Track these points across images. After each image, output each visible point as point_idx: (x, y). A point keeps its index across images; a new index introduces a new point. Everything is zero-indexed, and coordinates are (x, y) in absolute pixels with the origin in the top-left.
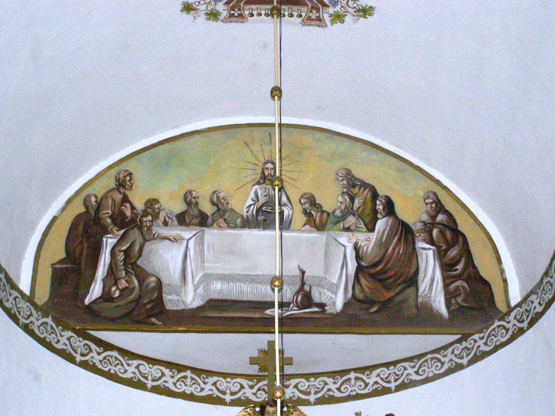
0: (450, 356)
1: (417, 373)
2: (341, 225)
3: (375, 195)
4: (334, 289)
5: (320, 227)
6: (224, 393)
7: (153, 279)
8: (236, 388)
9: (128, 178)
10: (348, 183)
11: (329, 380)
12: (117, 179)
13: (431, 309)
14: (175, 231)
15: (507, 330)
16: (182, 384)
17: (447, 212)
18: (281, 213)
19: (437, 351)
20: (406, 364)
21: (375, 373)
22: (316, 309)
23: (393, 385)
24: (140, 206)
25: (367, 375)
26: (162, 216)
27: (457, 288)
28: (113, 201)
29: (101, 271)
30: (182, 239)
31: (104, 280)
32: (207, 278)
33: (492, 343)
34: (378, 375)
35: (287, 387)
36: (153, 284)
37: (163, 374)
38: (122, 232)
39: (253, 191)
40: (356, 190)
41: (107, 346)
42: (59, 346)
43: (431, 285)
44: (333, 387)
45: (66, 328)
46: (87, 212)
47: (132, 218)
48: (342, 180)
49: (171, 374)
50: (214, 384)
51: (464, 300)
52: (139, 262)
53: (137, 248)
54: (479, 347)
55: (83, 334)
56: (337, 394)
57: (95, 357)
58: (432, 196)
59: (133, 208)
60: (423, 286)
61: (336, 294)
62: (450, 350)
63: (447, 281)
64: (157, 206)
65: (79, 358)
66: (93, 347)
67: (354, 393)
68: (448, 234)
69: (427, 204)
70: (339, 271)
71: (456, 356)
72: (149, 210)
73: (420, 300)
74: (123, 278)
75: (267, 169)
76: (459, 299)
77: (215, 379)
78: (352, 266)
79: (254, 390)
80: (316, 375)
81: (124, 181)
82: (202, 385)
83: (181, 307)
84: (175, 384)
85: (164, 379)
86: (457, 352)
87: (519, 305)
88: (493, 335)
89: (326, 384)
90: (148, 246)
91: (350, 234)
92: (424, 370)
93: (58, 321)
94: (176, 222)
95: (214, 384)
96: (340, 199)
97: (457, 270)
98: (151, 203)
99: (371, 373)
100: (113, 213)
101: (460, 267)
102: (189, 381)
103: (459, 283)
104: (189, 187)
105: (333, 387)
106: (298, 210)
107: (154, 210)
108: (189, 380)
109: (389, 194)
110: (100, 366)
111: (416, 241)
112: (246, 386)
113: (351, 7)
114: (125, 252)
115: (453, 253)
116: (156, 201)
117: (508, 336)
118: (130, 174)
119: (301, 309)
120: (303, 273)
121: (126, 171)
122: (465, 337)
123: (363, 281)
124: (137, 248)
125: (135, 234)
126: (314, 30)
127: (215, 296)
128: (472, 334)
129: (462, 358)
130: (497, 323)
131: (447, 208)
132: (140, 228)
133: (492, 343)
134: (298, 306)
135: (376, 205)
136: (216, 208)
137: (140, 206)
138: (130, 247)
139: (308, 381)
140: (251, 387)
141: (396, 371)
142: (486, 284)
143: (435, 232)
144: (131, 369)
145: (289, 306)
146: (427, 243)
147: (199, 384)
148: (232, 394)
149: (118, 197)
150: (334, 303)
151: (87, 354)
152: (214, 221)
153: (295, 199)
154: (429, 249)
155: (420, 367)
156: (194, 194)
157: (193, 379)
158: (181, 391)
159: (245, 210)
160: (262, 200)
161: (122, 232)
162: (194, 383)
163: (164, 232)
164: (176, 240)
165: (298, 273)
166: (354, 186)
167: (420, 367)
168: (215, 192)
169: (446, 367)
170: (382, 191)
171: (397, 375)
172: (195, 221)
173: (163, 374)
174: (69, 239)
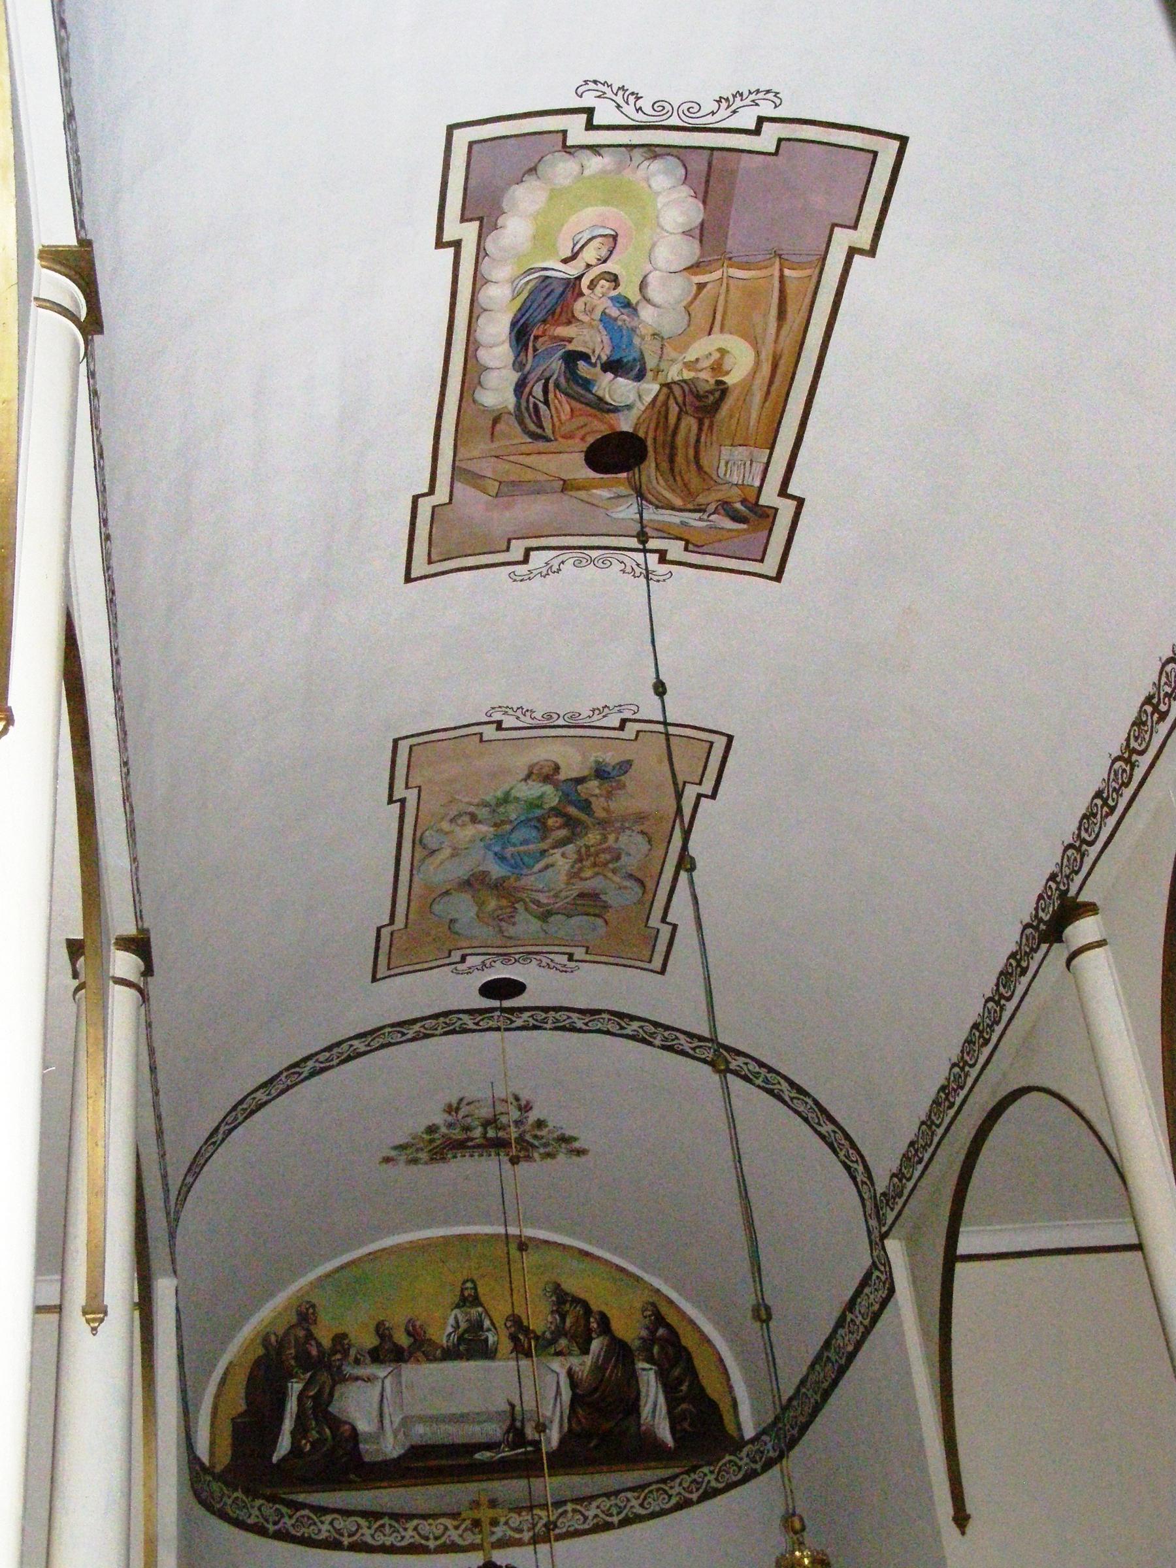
0: (677, 1489)
1: (642, 1505)
3: (588, 1311)
6: (427, 1539)
8: (438, 1533)
9: (311, 1311)
10: (557, 1298)
12: (299, 1314)
13: (655, 1437)
16: (381, 1534)
17: (669, 1326)
19: (664, 1481)
20: (629, 1495)
21: (595, 1504)
23: (615, 1520)
24: (326, 1343)
25: (586, 1506)
26: (353, 1352)
27: (684, 1412)
29: (288, 1425)
30: (376, 1378)
31: (292, 1433)
32: (407, 1421)
33: (602, 566)
34: (598, 1507)
36: (347, 1434)
38: (309, 1374)
39: (453, 1316)
41: (297, 1506)
42: (250, 1521)
43: (654, 1411)
45: (256, 1496)
47: (319, 1356)
48: (551, 1297)
49: (367, 1524)
50: (415, 1529)
54: (709, 1482)
55: (272, 1499)
58: (650, 1308)
59: (319, 1345)
60: (646, 1411)
62: (678, 1481)
63: (672, 1403)
64: (346, 1342)
65: (272, 1528)
66: (284, 1510)
67: (572, 1529)
68: (671, 1350)
69: (645, 1317)
70: (552, 1401)
71: (684, 1488)
74: (313, 1429)
75: (467, 1289)
76: (686, 1425)
77: (415, 1522)
79: (460, 1532)
81: (307, 1314)
83: (380, 1459)
85: (360, 1531)
87: (753, 1441)
88: (724, 1470)
91: (560, 1358)
92: (650, 1503)
93: (247, 1492)
94: (368, 1360)
95: (415, 1529)
96: (550, 1318)
97: (681, 1391)
98: (340, 1339)
99: (590, 1504)
100: (297, 1352)
102: (387, 1530)
103: (684, 1406)
106: (504, 1334)
107: (343, 1345)
108: (387, 1527)
109: (604, 1309)
110: (293, 1532)
111: (636, 1361)
112: (450, 1526)
114: (314, 1398)
115: (677, 1372)
116: (344, 1336)
117: (740, 1476)
118: (313, 1306)
119: (513, 1449)
121: (308, 1302)
122: (694, 1469)
125: (324, 1377)
128: (701, 1466)
129: (691, 1492)
133: (602, 566)
134: (508, 1445)
135: (589, 1323)
136: (412, 1340)
137: (326, 1343)
138: (319, 1391)
139: (519, 1515)
140: (457, 1528)
141: (618, 1502)
142: (713, 1406)
143: (656, 1350)
145: (500, 1447)
146: (648, 1363)
147: (398, 1532)
148: (436, 1538)
149: (301, 1333)
151: (279, 1521)
152: (411, 1355)
153: (500, 1323)
154: (651, 1369)
155: (645, 1499)
157: (391, 1526)
158: (381, 1542)
159: (444, 1341)
160: (463, 1325)
161: (309, 1374)
162: (394, 1532)
164: (368, 1379)
166: (564, 1303)
167: (645, 1499)
168: (409, 1321)
169: (674, 1501)
171: (620, 1507)
173: (359, 1526)
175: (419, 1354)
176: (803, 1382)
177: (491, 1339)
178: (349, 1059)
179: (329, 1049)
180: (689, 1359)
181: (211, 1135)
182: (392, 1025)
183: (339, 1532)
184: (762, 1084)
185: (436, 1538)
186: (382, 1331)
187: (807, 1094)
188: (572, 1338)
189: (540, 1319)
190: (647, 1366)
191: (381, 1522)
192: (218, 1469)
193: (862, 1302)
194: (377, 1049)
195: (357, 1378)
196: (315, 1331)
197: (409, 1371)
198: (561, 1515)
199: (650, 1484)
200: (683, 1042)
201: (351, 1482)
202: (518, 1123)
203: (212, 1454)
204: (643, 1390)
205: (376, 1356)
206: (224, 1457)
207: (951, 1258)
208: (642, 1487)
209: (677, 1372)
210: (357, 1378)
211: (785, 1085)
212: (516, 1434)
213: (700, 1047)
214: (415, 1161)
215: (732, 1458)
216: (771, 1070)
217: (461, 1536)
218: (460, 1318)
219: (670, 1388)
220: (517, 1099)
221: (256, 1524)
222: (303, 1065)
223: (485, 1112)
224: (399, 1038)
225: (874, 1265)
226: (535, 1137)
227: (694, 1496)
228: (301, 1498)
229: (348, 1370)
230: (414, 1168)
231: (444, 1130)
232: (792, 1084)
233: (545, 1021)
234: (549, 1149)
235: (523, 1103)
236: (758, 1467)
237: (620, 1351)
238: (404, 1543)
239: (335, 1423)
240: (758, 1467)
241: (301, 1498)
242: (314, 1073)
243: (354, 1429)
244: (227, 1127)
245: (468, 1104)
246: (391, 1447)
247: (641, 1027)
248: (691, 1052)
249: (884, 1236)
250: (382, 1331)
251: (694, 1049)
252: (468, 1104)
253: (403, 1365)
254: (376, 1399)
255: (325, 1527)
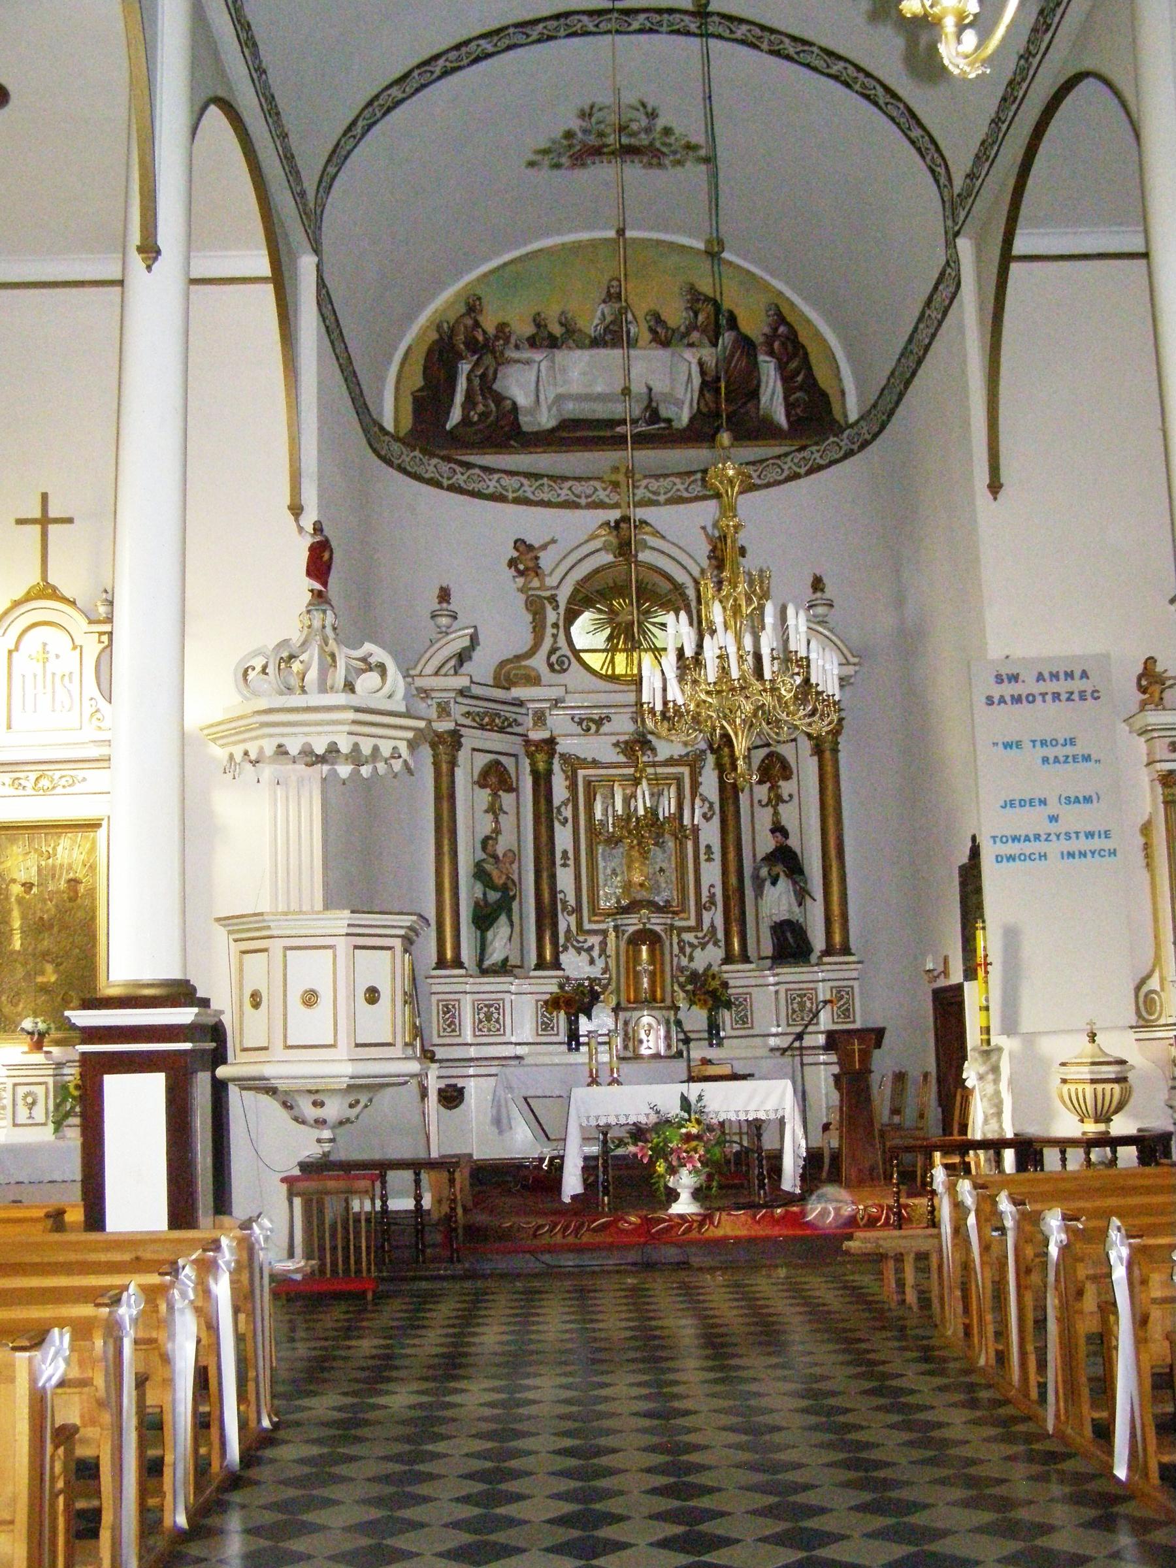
0: (790, 464)
2: (686, 341)
4: (679, 404)
5: (665, 344)
6: (579, 497)
7: (508, 402)
8: (589, 492)
11: (677, 480)
12: (467, 304)
14: (527, 354)
15: (841, 448)
18: (628, 332)
19: (779, 457)
22: (663, 425)
24: (491, 330)
26: (513, 340)
27: (797, 400)
28: (466, 327)
29: (459, 398)
35: (638, 487)
37: (522, 485)
38: (476, 357)
40: (700, 305)
41: (468, 466)
42: (427, 476)
43: (772, 400)
44: (681, 487)
45: (432, 455)
46: (441, 338)
50: (570, 489)
51: (803, 411)
52: (495, 387)
53: (491, 371)
55: (448, 459)
56: (686, 495)
57: (460, 479)
59: (484, 332)
60: (764, 399)
61: (681, 408)
62: (789, 458)
65: (446, 483)
66: (458, 469)
68: (790, 348)
72: (501, 334)
73: (761, 412)
76: (799, 411)
77: (570, 483)
78: (697, 381)
80: (666, 476)
81: (474, 305)
82: (559, 491)
83: (536, 429)
84: (533, 493)
86: (796, 461)
89: (675, 484)
90: (502, 371)
91: (694, 350)
93: (424, 451)
94: (527, 346)
95: (570, 489)
96: (684, 314)
98: (502, 327)
101: (800, 378)
102: (546, 489)
103: (798, 394)
104: (537, 309)
105: (681, 487)
106: (644, 327)
107: (504, 333)
112: (598, 487)
113: (668, 541)
115: (793, 365)
118: (479, 299)
120: (650, 390)
122: (803, 448)
123: (707, 395)
124: (491, 371)
125: (488, 359)
126: (655, 173)
127: (567, 416)
130: (832, 439)
131: (789, 319)
132: (493, 352)
136: (563, 330)
137: (491, 330)
142: (824, 395)
143: (776, 345)
144: (492, 484)
148: (587, 497)
150: (680, 419)
153: (640, 315)
156: (543, 316)
157: (550, 486)
160: (609, 319)
161: (476, 357)
163: (515, 355)
164: (528, 362)
165: (645, 390)
166: (698, 300)
170: (726, 305)
172: (545, 343)
174: (426, 369)
175: (571, 341)
176: (892, 373)
177: (633, 330)
178: (477, 60)
179: (457, 47)
180: (806, 354)
181: (349, 128)
182: (516, 26)
183: (504, 488)
184: (860, 90)
185: (587, 497)
186: (539, 322)
187: (899, 99)
188: (704, 332)
189: (676, 315)
190: (768, 358)
191: (540, 482)
192: (402, 434)
193: (937, 298)
194: (504, 51)
195: (518, 361)
196: (481, 319)
197: (560, 356)
198: (692, 482)
199: (767, 460)
200: (787, 46)
201: (513, 447)
202: (648, 130)
203: (397, 420)
204: (764, 379)
205: (533, 342)
206: (407, 422)
207: (1007, 258)
208: (761, 461)
209: (793, 365)
210: (518, 361)
211: (880, 91)
212: (653, 415)
213: (804, 51)
214: (557, 166)
215: (835, 439)
216: (868, 75)
217: (608, 496)
218: (606, 311)
219: (787, 379)
220: (644, 105)
221: (432, 479)
222: (433, 63)
223: (613, 118)
224: (522, 39)
225: (948, 263)
226: (665, 144)
227: (802, 471)
228: (472, 459)
229: (512, 354)
230: (556, 172)
231: (580, 135)
232: (887, 89)
233: (660, 23)
234: (678, 156)
235: (650, 110)
236: (855, 447)
237: (746, 345)
238: (560, 499)
239: (499, 399)
240: (855, 447)
241: (472, 459)
242: (446, 73)
243: (514, 404)
244: (365, 122)
245: (600, 110)
246: (546, 420)
247: (750, 31)
248: (796, 56)
249: (957, 234)
250: (539, 322)
251: (798, 53)
252: (600, 110)
253: (556, 351)
254: (534, 379)
255: (492, 484)
